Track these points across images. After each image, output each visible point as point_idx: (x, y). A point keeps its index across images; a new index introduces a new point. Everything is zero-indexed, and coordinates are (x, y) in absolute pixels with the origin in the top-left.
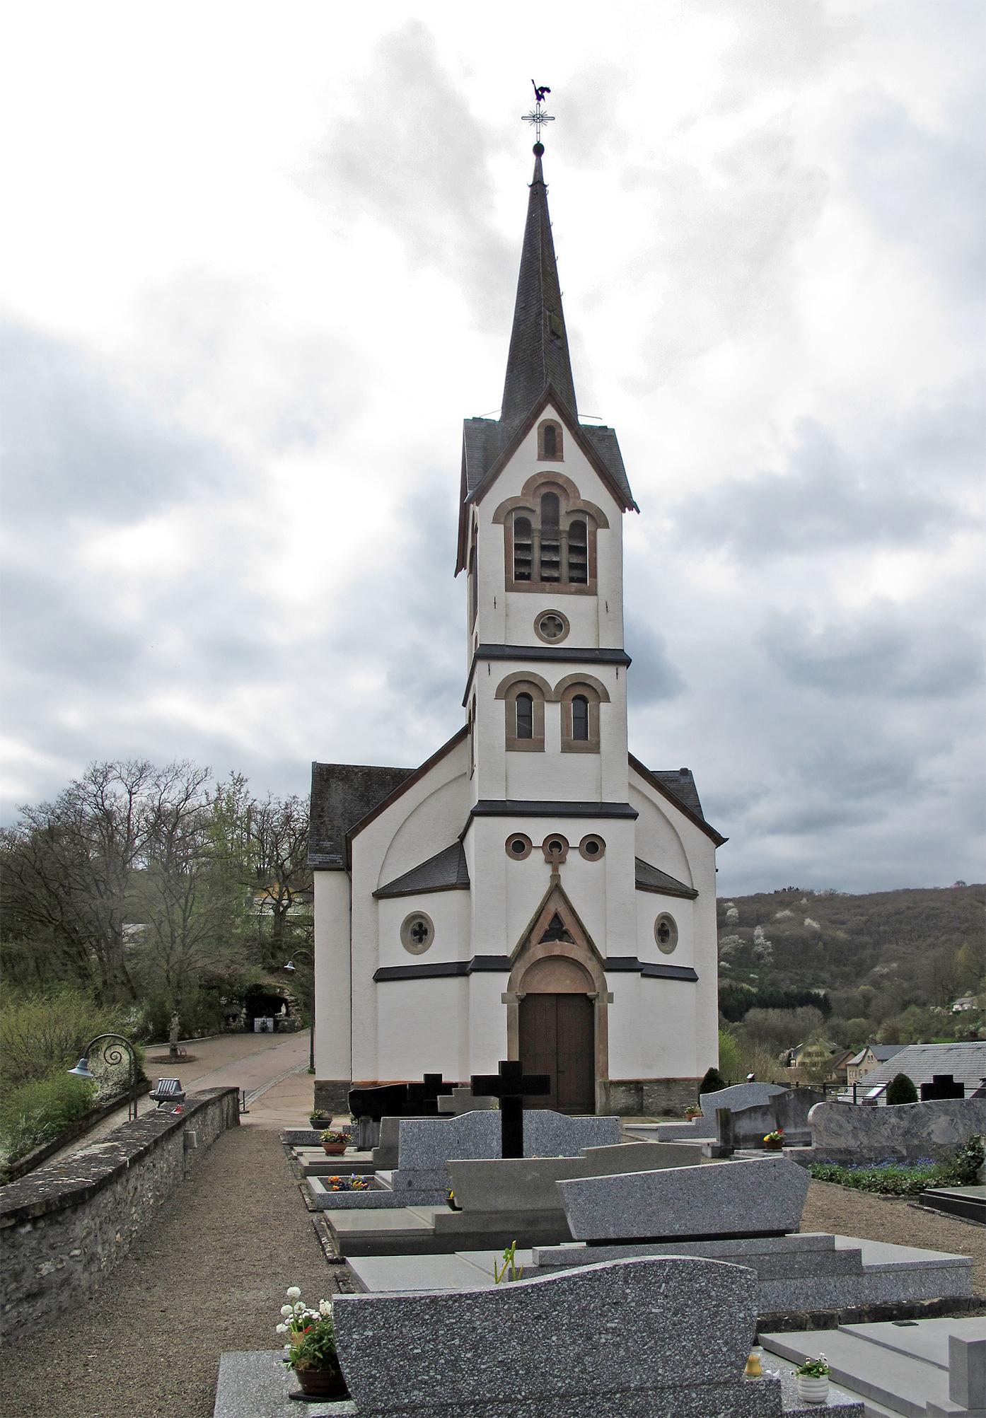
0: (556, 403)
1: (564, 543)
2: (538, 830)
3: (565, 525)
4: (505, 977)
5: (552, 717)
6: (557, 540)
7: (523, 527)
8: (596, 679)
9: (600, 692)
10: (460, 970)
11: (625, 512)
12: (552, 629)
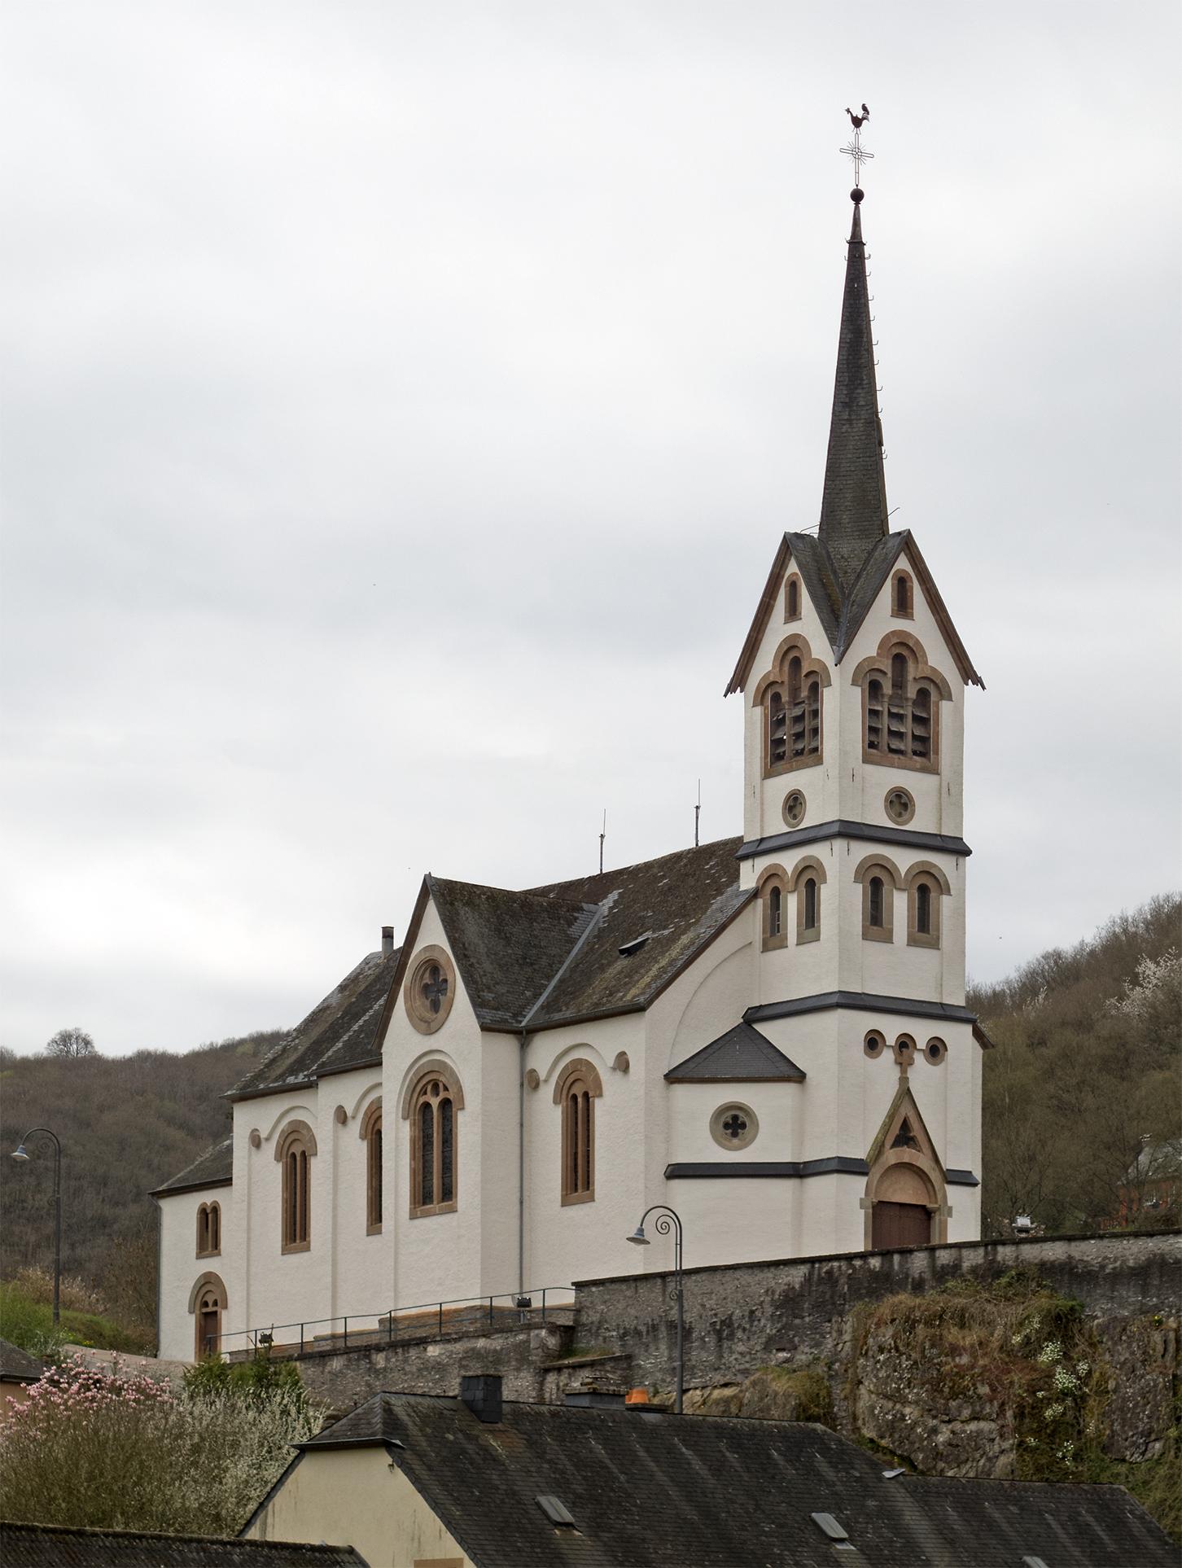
0: (911, 553)
1: (908, 711)
2: (892, 1027)
3: (912, 692)
4: (861, 1182)
5: (900, 905)
6: (902, 707)
7: (874, 689)
8: (940, 869)
9: (942, 884)
10: (798, 1171)
11: (967, 685)
12: (897, 807)
